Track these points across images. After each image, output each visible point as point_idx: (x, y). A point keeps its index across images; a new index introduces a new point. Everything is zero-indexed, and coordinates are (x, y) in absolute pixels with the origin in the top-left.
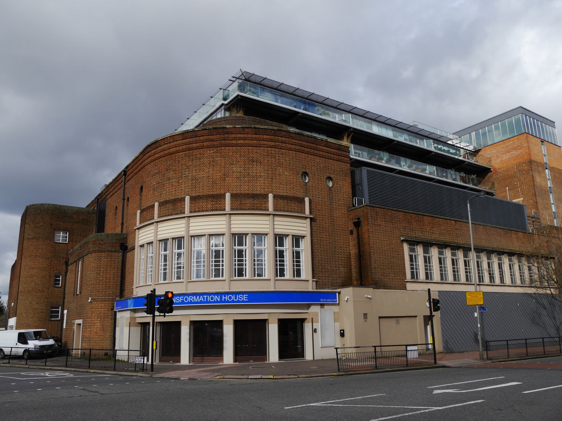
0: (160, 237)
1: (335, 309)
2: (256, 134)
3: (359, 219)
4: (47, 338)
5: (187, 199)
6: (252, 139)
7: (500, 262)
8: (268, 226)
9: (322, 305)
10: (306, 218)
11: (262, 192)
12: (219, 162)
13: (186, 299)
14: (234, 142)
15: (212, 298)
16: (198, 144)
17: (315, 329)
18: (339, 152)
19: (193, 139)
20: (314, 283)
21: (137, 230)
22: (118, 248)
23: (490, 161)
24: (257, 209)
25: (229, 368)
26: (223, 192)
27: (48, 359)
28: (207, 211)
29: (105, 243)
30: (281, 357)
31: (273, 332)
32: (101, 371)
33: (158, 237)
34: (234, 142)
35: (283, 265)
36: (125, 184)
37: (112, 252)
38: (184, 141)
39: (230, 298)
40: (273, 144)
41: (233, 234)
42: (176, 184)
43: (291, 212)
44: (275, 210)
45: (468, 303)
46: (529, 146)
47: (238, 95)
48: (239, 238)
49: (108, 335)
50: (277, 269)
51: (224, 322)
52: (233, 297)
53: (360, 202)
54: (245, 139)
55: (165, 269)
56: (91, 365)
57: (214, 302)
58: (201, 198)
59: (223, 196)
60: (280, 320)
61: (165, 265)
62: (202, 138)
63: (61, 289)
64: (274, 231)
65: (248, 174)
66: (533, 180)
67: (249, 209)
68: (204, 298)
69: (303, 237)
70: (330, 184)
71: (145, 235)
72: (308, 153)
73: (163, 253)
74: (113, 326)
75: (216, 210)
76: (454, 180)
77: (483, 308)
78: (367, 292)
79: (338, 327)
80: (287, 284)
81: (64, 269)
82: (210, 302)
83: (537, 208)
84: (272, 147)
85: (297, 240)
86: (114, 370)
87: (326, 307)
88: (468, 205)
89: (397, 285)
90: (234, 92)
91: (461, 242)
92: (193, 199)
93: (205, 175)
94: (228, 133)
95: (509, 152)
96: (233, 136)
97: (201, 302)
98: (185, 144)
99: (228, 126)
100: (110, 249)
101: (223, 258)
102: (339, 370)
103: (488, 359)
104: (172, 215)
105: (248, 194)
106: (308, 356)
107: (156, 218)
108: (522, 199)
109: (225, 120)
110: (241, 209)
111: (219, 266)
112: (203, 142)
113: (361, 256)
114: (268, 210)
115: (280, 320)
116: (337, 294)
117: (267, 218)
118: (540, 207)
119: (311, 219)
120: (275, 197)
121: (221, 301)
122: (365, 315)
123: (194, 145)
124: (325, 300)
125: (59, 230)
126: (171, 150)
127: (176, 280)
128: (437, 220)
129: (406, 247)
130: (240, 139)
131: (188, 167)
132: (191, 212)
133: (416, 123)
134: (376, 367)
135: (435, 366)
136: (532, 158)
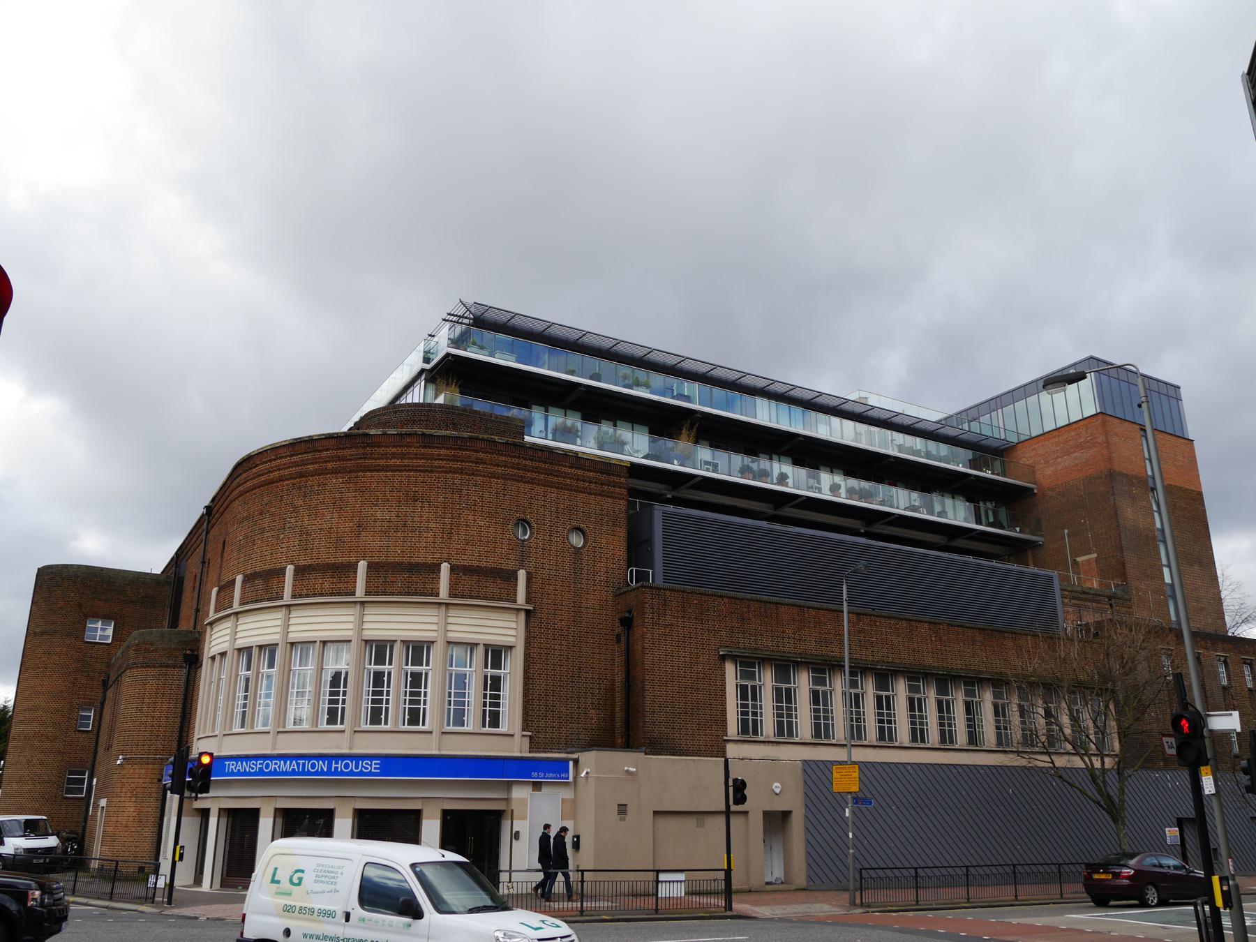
0: (241, 643)
1: (567, 794)
2: (425, 447)
3: (630, 612)
4: (46, 834)
6: (417, 457)
7: (969, 699)
8: (435, 627)
9: (537, 786)
11: (429, 560)
12: (351, 501)
13: (267, 766)
14: (382, 462)
15: (313, 766)
17: (517, 833)
18: (604, 477)
19: (310, 456)
20: (527, 740)
21: (208, 628)
22: (181, 658)
23: (1034, 472)
24: (415, 594)
26: (353, 559)
28: (321, 595)
29: (156, 650)
33: (291, 635)
34: (382, 462)
37: (167, 666)
38: (294, 459)
39: (347, 766)
40: (458, 465)
41: (366, 641)
42: (274, 541)
43: (485, 598)
45: (836, 788)
46: (1107, 442)
47: (448, 355)
48: (380, 649)
49: (148, 831)
51: (337, 813)
52: (352, 765)
54: (402, 456)
55: (245, 706)
57: (316, 773)
58: (314, 569)
59: (353, 567)
60: (445, 813)
61: (246, 698)
62: (324, 454)
63: (91, 736)
65: (405, 525)
66: (1116, 516)
67: (400, 594)
68: (298, 765)
70: (577, 540)
71: (218, 640)
73: (243, 673)
74: (158, 815)
75: (339, 594)
78: (628, 761)
80: (472, 743)
81: (100, 695)
84: (454, 471)
85: (496, 654)
86: (111, 899)
87: (545, 789)
88: (845, 587)
90: (442, 346)
91: (871, 658)
92: (299, 571)
93: (324, 526)
94: (371, 445)
95: (1068, 453)
96: (382, 450)
97: (293, 773)
98: (295, 464)
99: (373, 432)
100: (165, 660)
101: (389, 686)
103: (862, 905)
104: (261, 601)
105: (401, 563)
107: (236, 607)
108: (1095, 555)
110: (385, 593)
113: (631, 687)
114: (438, 595)
115: (445, 813)
116: (571, 763)
117: (433, 611)
118: (1131, 571)
119: (528, 612)
120: (453, 569)
121: (329, 773)
122: (622, 808)
123: (311, 467)
124: (541, 775)
125: (96, 616)
126: (272, 475)
128: (813, 612)
129: (731, 672)
130: (394, 456)
131: (296, 510)
132: (368, 593)
134: (582, 911)
135: (728, 913)
136: (1116, 468)
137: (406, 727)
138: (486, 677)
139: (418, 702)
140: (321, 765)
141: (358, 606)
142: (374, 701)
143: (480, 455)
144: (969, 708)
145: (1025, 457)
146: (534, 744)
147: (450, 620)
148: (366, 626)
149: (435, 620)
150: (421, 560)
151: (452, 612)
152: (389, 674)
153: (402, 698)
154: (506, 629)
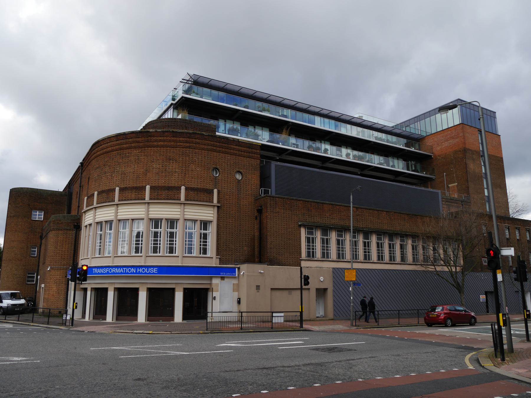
0: (97, 220)
1: (235, 281)
2: (173, 137)
3: (261, 207)
4: (20, 298)
5: (117, 189)
6: (170, 141)
7: (402, 243)
8: (179, 213)
10: (214, 206)
11: (176, 185)
13: (110, 270)
14: (155, 143)
15: (130, 270)
16: (127, 145)
17: (215, 297)
18: (250, 150)
19: (124, 141)
20: (218, 259)
22: (72, 226)
23: (432, 148)
24: (171, 199)
25: (141, 325)
26: (144, 185)
27: (21, 315)
28: (131, 200)
29: (62, 223)
30: (184, 318)
31: (179, 297)
32: (37, 325)
33: (119, 217)
34: (155, 143)
35: (206, 245)
36: (82, 174)
37: (67, 230)
38: (117, 142)
39: (144, 270)
40: (188, 145)
41: (150, 219)
42: (110, 177)
43: (200, 201)
44: (186, 200)
45: (346, 279)
46: (464, 136)
47: (182, 97)
48: (156, 223)
49: (62, 297)
50: (200, 248)
51: (140, 289)
52: (146, 270)
53: (266, 192)
54: (164, 141)
55: (100, 246)
56: (50, 321)
57: (131, 273)
59: (144, 188)
60: (185, 289)
61: (100, 243)
62: (130, 140)
63: (36, 258)
64: (184, 217)
67: (164, 199)
68: (123, 270)
69: (211, 222)
70: (239, 177)
71: (88, 219)
72: (219, 152)
73: (99, 232)
75: (138, 199)
76: (392, 167)
77: (359, 284)
78: (260, 268)
79: (236, 295)
81: (39, 242)
82: (128, 273)
83: (468, 193)
84: (186, 147)
85: (205, 224)
86: (48, 324)
87: (226, 280)
89: (291, 263)
90: (180, 94)
92: (121, 190)
93: (131, 171)
94: (150, 136)
95: (447, 141)
96: (155, 138)
97: (121, 273)
98: (118, 144)
99: (151, 130)
101: (142, 238)
102: (207, 329)
105: (164, 187)
106: (209, 320)
107: (95, 205)
109: (161, 122)
110: (158, 199)
111: (157, 244)
112: (131, 143)
114: (180, 200)
115: (185, 289)
116: (237, 269)
117: (179, 207)
119: (218, 207)
120: (187, 189)
121: (136, 273)
122: (258, 287)
123: (125, 146)
124: (224, 274)
125: (36, 209)
127: (134, 254)
129: (303, 232)
130: (160, 141)
132: (119, 201)
133: (361, 115)
134: (241, 328)
136: (467, 147)
137: (168, 254)
138: (201, 234)
139: (173, 244)
140: (133, 270)
141: (183, 205)
142: (154, 244)
143: (197, 140)
144: (402, 247)
145: (429, 142)
146: (221, 262)
147: (186, 210)
148: (150, 213)
149: (179, 210)
150: (173, 185)
151: (186, 207)
152: (160, 233)
153: (166, 242)
154: (209, 214)
